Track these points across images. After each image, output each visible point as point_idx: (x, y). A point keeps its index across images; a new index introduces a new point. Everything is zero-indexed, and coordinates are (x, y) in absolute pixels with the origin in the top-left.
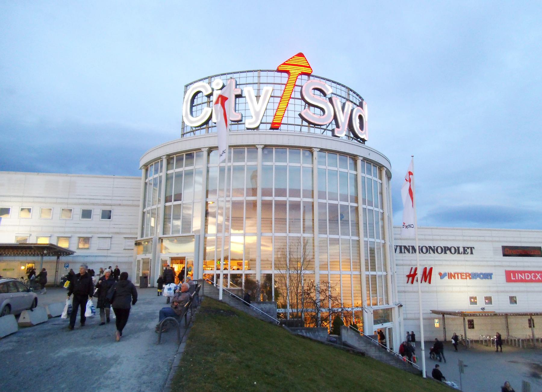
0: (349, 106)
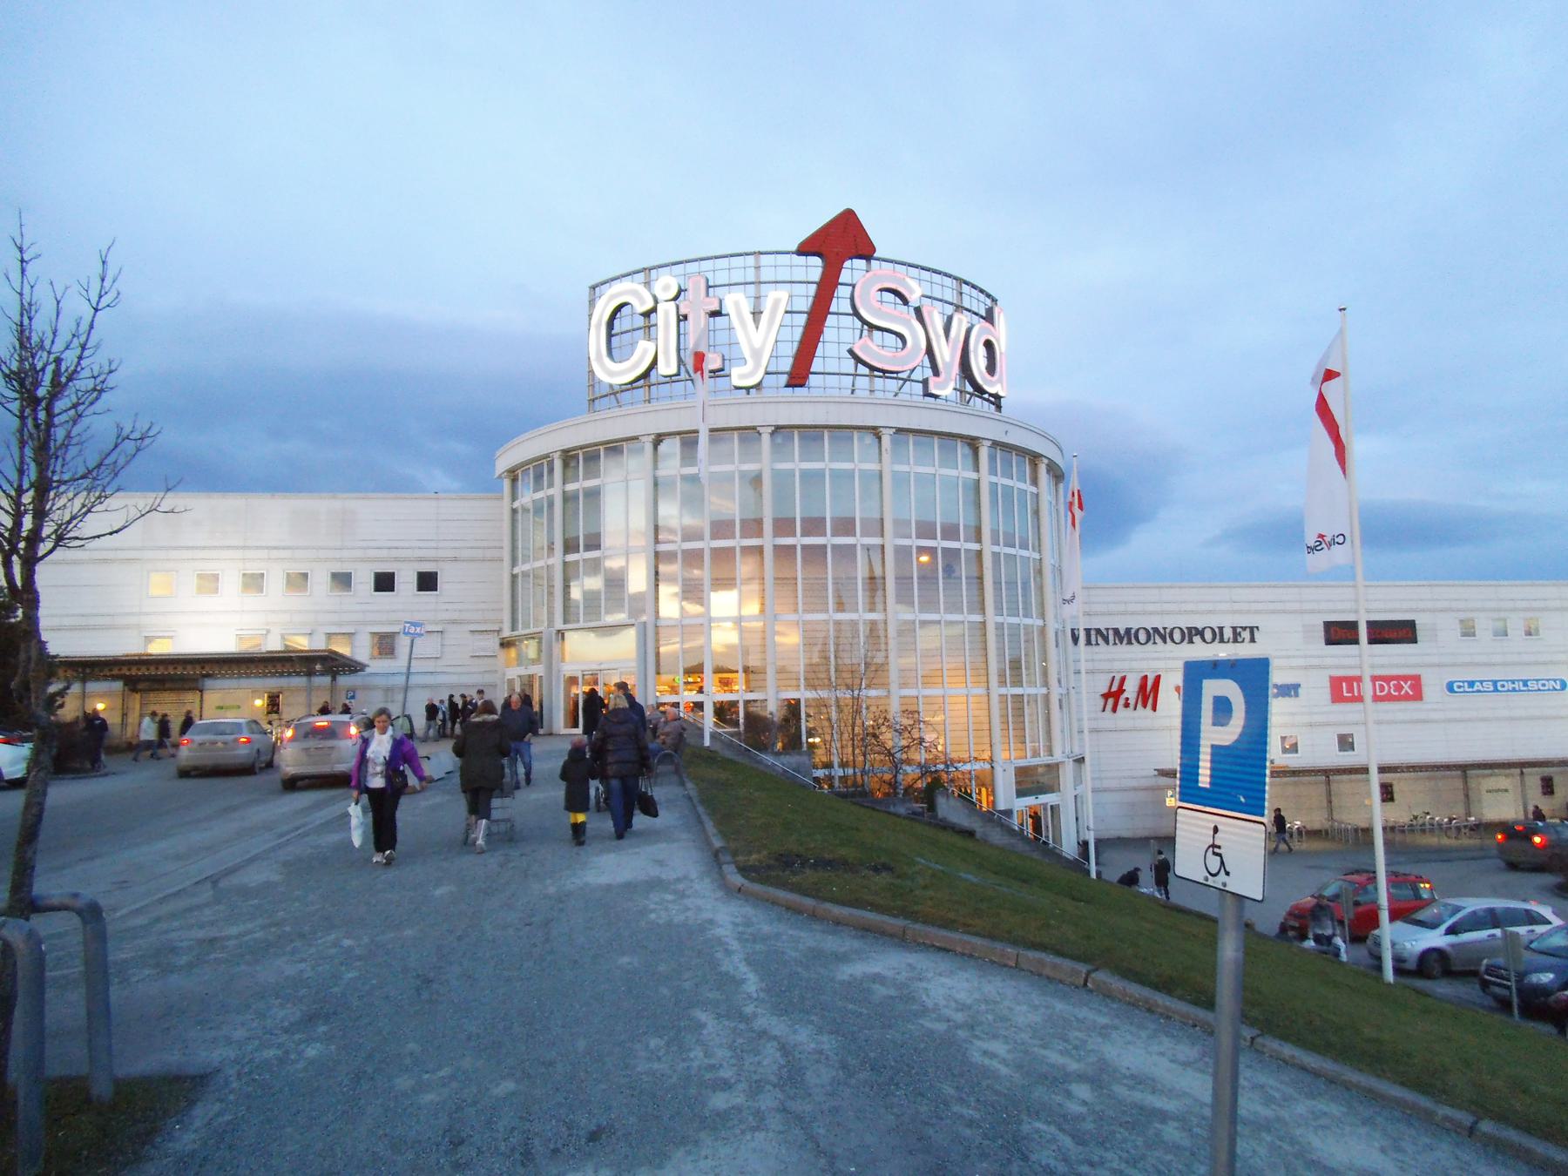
0: (960, 321)
